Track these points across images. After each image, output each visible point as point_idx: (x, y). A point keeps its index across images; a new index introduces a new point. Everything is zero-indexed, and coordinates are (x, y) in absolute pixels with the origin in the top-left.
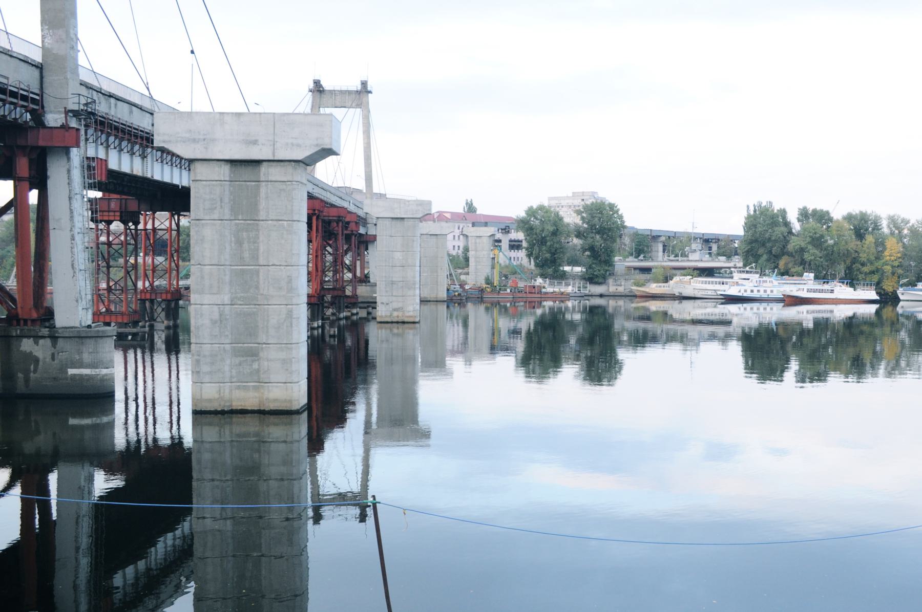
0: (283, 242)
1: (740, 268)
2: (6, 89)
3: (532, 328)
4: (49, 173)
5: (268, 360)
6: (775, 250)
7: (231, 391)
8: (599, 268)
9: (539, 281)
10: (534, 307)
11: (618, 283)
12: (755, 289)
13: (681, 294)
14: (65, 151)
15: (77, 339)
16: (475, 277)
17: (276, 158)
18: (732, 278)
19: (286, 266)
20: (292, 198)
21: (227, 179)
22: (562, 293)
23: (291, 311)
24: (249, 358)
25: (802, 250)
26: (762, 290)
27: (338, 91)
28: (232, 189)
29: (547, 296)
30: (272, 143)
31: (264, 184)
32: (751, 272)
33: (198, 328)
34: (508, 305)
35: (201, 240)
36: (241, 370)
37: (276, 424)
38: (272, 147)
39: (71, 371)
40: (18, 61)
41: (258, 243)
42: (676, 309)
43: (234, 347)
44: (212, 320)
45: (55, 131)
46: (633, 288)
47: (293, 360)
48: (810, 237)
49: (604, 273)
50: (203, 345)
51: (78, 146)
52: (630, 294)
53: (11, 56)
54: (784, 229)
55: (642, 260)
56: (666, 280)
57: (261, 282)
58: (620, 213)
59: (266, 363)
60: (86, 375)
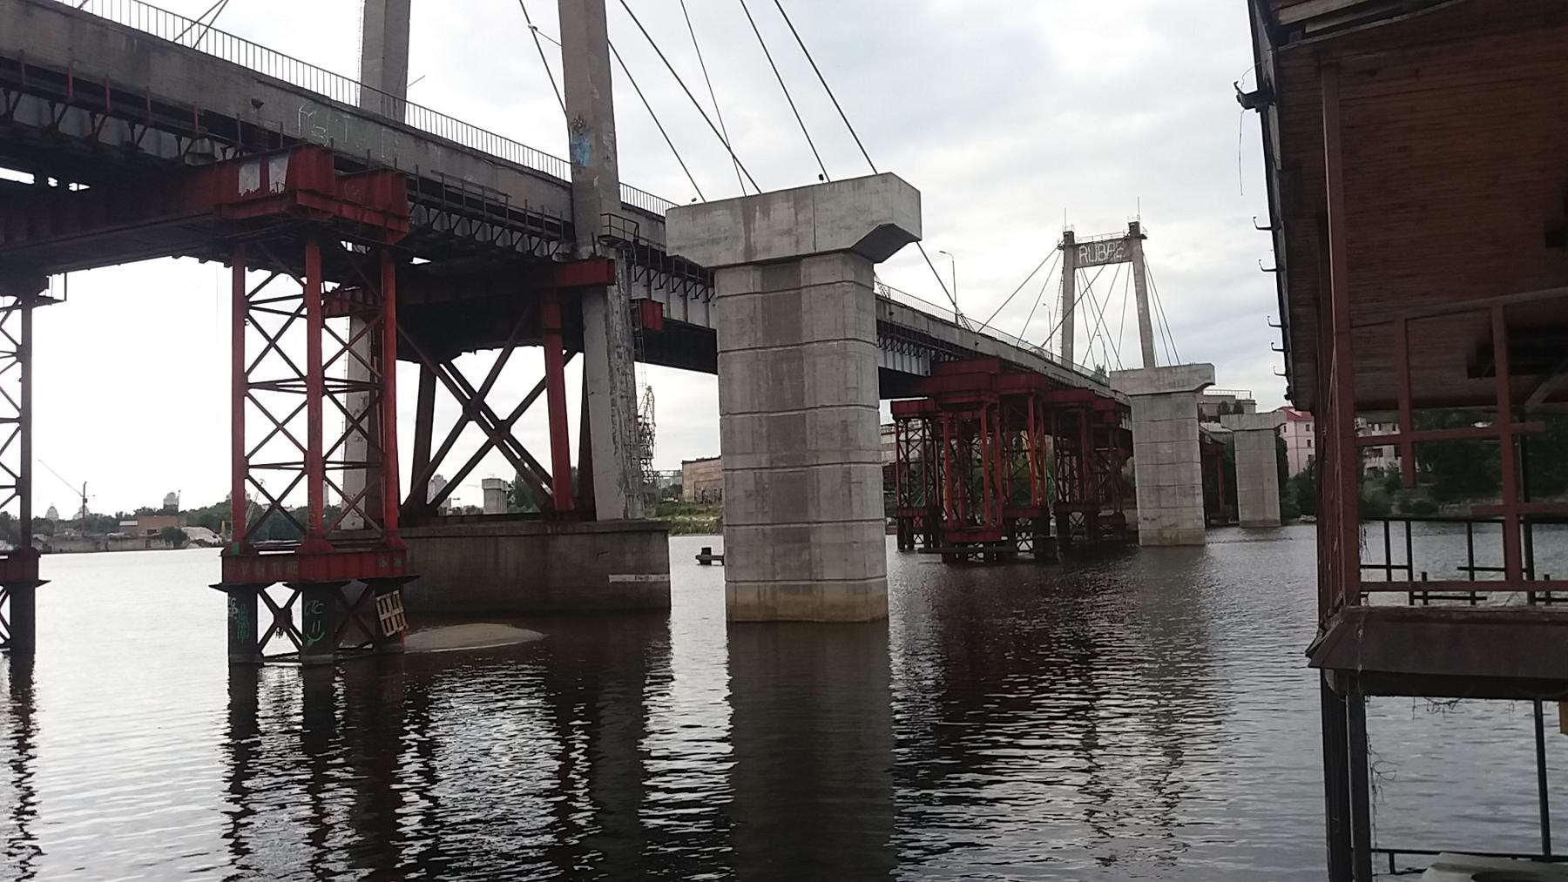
2: (542, 220)
23: (849, 473)
31: (805, 290)
39: (613, 578)
40: (532, 179)
41: (803, 377)
44: (746, 491)
47: (855, 545)
50: (736, 528)
57: (808, 432)
59: (818, 551)
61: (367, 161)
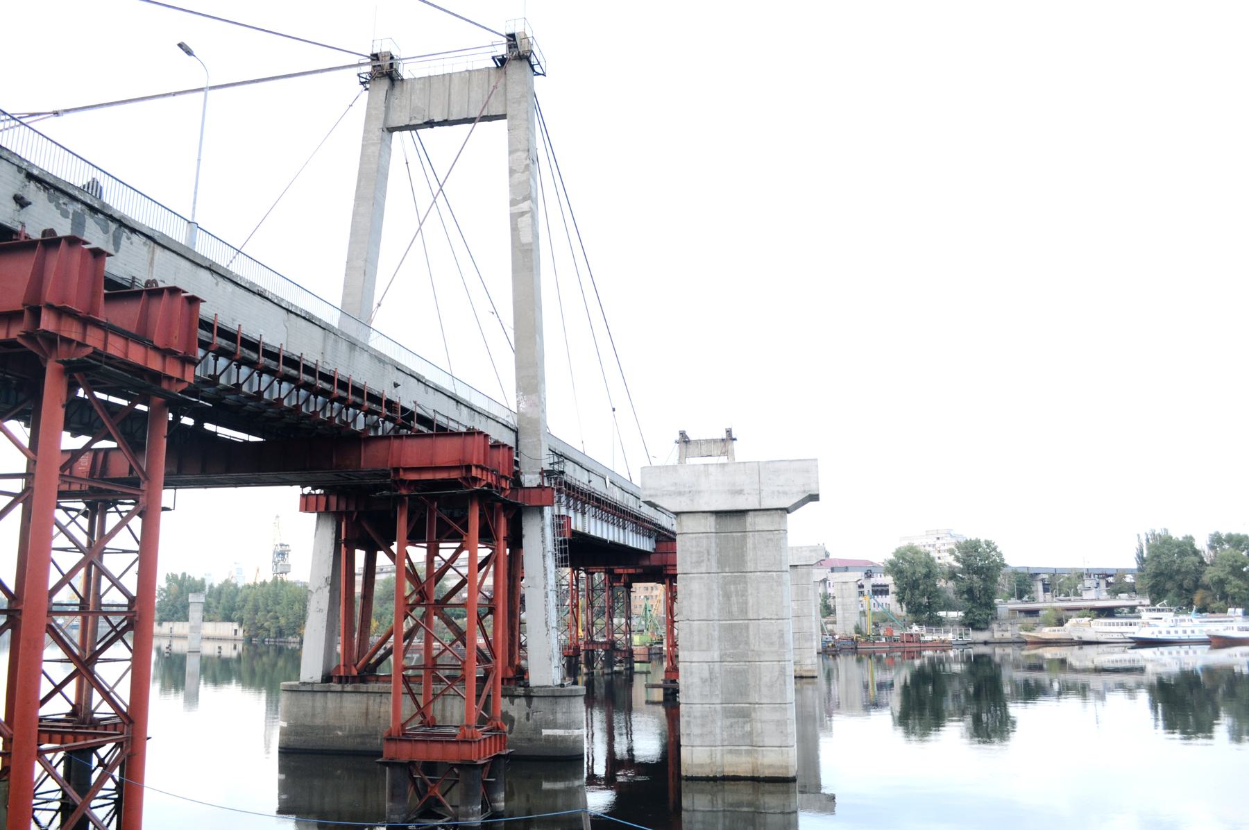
0: (773, 593)
1: (1148, 606)
3: (908, 681)
4: (524, 532)
5: (761, 722)
6: (1186, 583)
7: (722, 755)
8: (981, 612)
9: (915, 629)
10: (913, 658)
11: (1004, 628)
12: (1172, 630)
13: (1081, 638)
14: (539, 510)
15: (550, 699)
16: (844, 626)
17: (763, 507)
18: (1139, 617)
19: (777, 619)
20: (781, 548)
21: (713, 530)
22: (944, 642)
23: (784, 668)
24: (740, 720)
25: (1221, 582)
26: (1180, 630)
27: (704, 440)
28: (717, 540)
29: (927, 645)
30: (758, 492)
31: (751, 534)
32: (1163, 610)
33: (687, 687)
34: (884, 655)
35: (689, 594)
36: (733, 732)
37: (771, 793)
38: (758, 496)
39: (545, 732)
41: (747, 596)
42: (1075, 657)
43: (725, 707)
45: (532, 490)
46: (1022, 633)
48: (1230, 566)
49: (986, 617)
51: (552, 505)
52: (1018, 640)
53: (498, 422)
54: (1196, 559)
55: (1026, 602)
56: (1060, 623)
57: (751, 637)
58: (998, 550)
59: (759, 725)
60: (560, 736)
61: (259, 342)
